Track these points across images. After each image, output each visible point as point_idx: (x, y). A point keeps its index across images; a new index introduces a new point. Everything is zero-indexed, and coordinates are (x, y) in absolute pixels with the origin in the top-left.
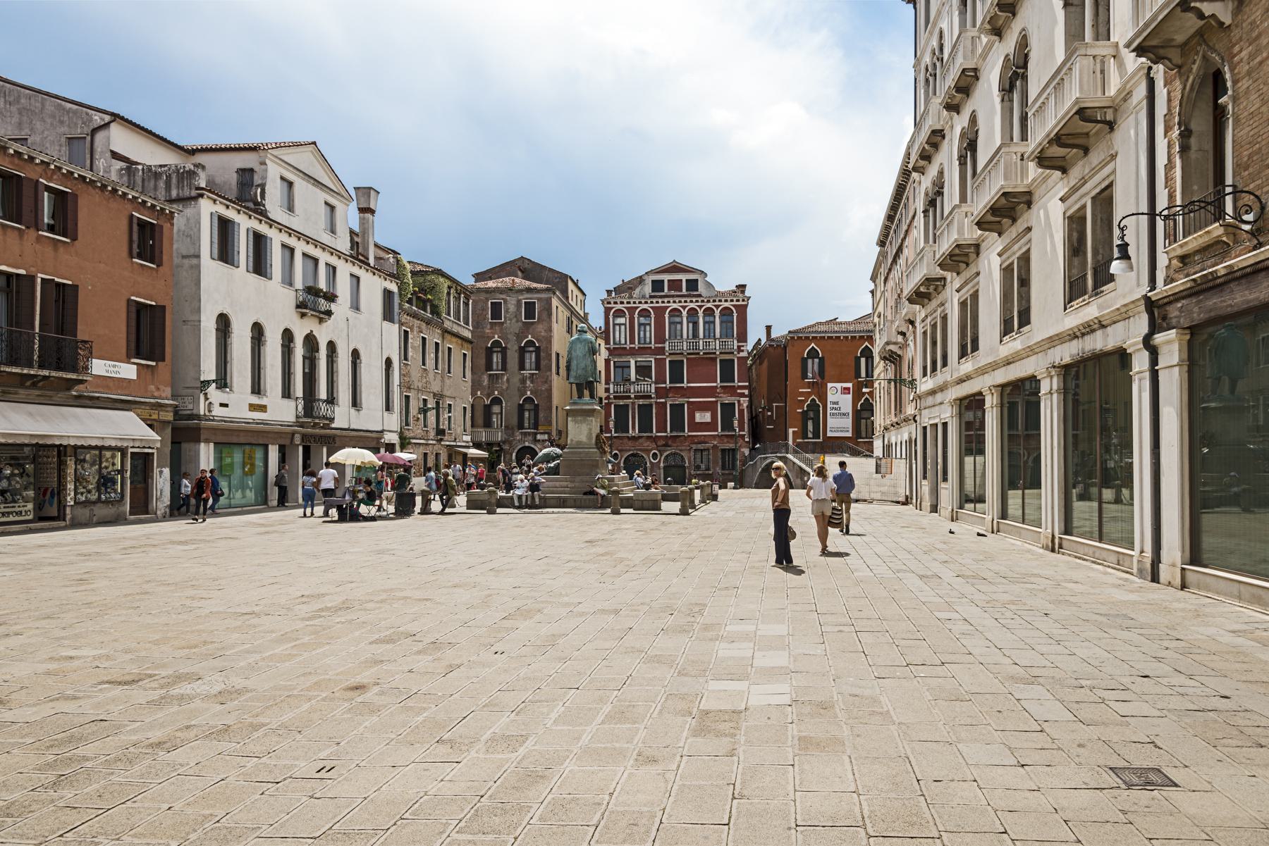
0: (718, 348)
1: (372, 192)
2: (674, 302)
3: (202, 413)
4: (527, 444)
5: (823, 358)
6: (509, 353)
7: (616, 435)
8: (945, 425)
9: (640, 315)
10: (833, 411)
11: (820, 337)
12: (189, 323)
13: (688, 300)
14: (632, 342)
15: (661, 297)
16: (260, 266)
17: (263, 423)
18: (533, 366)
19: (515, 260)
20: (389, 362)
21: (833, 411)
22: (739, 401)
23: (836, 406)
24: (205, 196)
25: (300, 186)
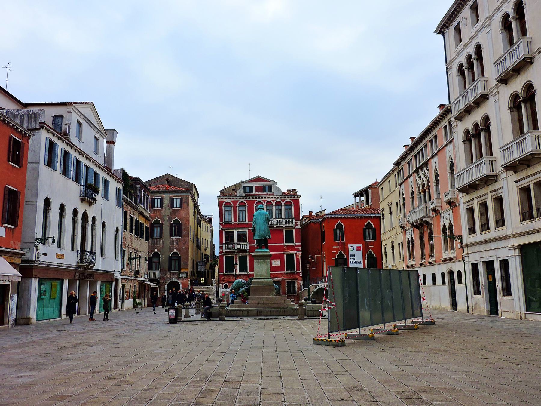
0: (284, 224)
1: (115, 132)
2: (259, 198)
3: (34, 259)
4: (174, 280)
5: (374, 228)
6: (164, 227)
7: (226, 274)
8: (504, 264)
9: (240, 206)
10: (352, 260)
11: (343, 217)
12: (29, 203)
13: (267, 197)
14: (235, 220)
15: (251, 195)
16: (65, 172)
17: (62, 265)
18: (158, 235)
19: (163, 176)
20: (117, 230)
21: (352, 260)
22: (296, 254)
23: (354, 257)
24: (45, 128)
25: (85, 125)
